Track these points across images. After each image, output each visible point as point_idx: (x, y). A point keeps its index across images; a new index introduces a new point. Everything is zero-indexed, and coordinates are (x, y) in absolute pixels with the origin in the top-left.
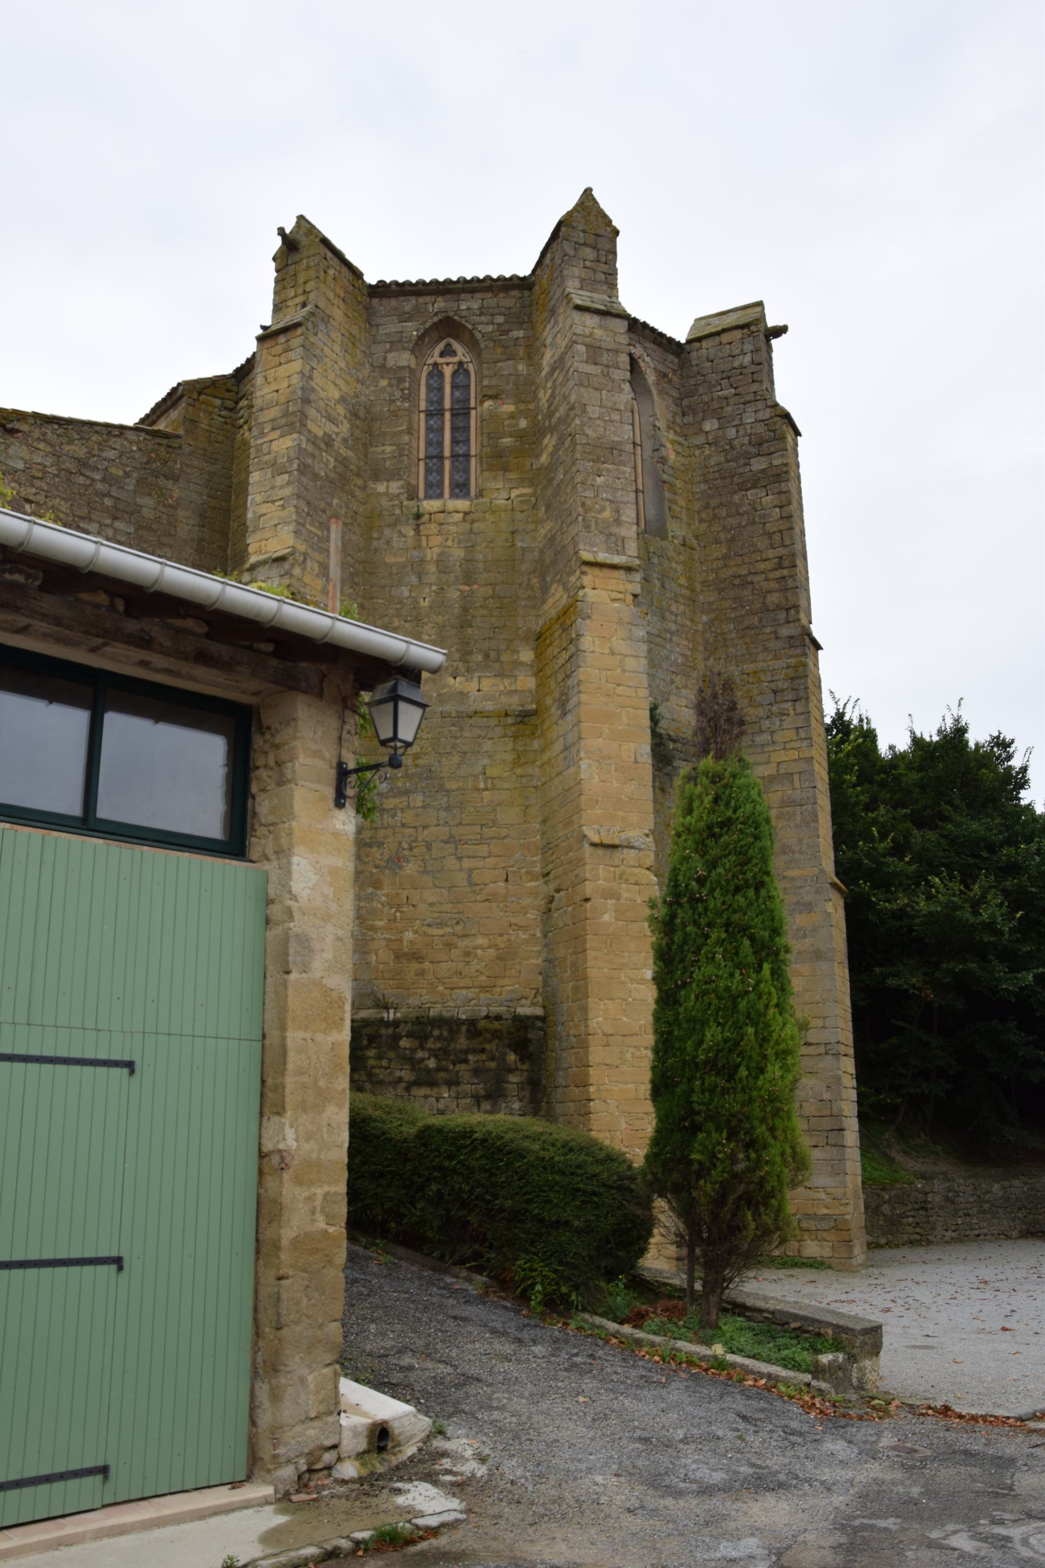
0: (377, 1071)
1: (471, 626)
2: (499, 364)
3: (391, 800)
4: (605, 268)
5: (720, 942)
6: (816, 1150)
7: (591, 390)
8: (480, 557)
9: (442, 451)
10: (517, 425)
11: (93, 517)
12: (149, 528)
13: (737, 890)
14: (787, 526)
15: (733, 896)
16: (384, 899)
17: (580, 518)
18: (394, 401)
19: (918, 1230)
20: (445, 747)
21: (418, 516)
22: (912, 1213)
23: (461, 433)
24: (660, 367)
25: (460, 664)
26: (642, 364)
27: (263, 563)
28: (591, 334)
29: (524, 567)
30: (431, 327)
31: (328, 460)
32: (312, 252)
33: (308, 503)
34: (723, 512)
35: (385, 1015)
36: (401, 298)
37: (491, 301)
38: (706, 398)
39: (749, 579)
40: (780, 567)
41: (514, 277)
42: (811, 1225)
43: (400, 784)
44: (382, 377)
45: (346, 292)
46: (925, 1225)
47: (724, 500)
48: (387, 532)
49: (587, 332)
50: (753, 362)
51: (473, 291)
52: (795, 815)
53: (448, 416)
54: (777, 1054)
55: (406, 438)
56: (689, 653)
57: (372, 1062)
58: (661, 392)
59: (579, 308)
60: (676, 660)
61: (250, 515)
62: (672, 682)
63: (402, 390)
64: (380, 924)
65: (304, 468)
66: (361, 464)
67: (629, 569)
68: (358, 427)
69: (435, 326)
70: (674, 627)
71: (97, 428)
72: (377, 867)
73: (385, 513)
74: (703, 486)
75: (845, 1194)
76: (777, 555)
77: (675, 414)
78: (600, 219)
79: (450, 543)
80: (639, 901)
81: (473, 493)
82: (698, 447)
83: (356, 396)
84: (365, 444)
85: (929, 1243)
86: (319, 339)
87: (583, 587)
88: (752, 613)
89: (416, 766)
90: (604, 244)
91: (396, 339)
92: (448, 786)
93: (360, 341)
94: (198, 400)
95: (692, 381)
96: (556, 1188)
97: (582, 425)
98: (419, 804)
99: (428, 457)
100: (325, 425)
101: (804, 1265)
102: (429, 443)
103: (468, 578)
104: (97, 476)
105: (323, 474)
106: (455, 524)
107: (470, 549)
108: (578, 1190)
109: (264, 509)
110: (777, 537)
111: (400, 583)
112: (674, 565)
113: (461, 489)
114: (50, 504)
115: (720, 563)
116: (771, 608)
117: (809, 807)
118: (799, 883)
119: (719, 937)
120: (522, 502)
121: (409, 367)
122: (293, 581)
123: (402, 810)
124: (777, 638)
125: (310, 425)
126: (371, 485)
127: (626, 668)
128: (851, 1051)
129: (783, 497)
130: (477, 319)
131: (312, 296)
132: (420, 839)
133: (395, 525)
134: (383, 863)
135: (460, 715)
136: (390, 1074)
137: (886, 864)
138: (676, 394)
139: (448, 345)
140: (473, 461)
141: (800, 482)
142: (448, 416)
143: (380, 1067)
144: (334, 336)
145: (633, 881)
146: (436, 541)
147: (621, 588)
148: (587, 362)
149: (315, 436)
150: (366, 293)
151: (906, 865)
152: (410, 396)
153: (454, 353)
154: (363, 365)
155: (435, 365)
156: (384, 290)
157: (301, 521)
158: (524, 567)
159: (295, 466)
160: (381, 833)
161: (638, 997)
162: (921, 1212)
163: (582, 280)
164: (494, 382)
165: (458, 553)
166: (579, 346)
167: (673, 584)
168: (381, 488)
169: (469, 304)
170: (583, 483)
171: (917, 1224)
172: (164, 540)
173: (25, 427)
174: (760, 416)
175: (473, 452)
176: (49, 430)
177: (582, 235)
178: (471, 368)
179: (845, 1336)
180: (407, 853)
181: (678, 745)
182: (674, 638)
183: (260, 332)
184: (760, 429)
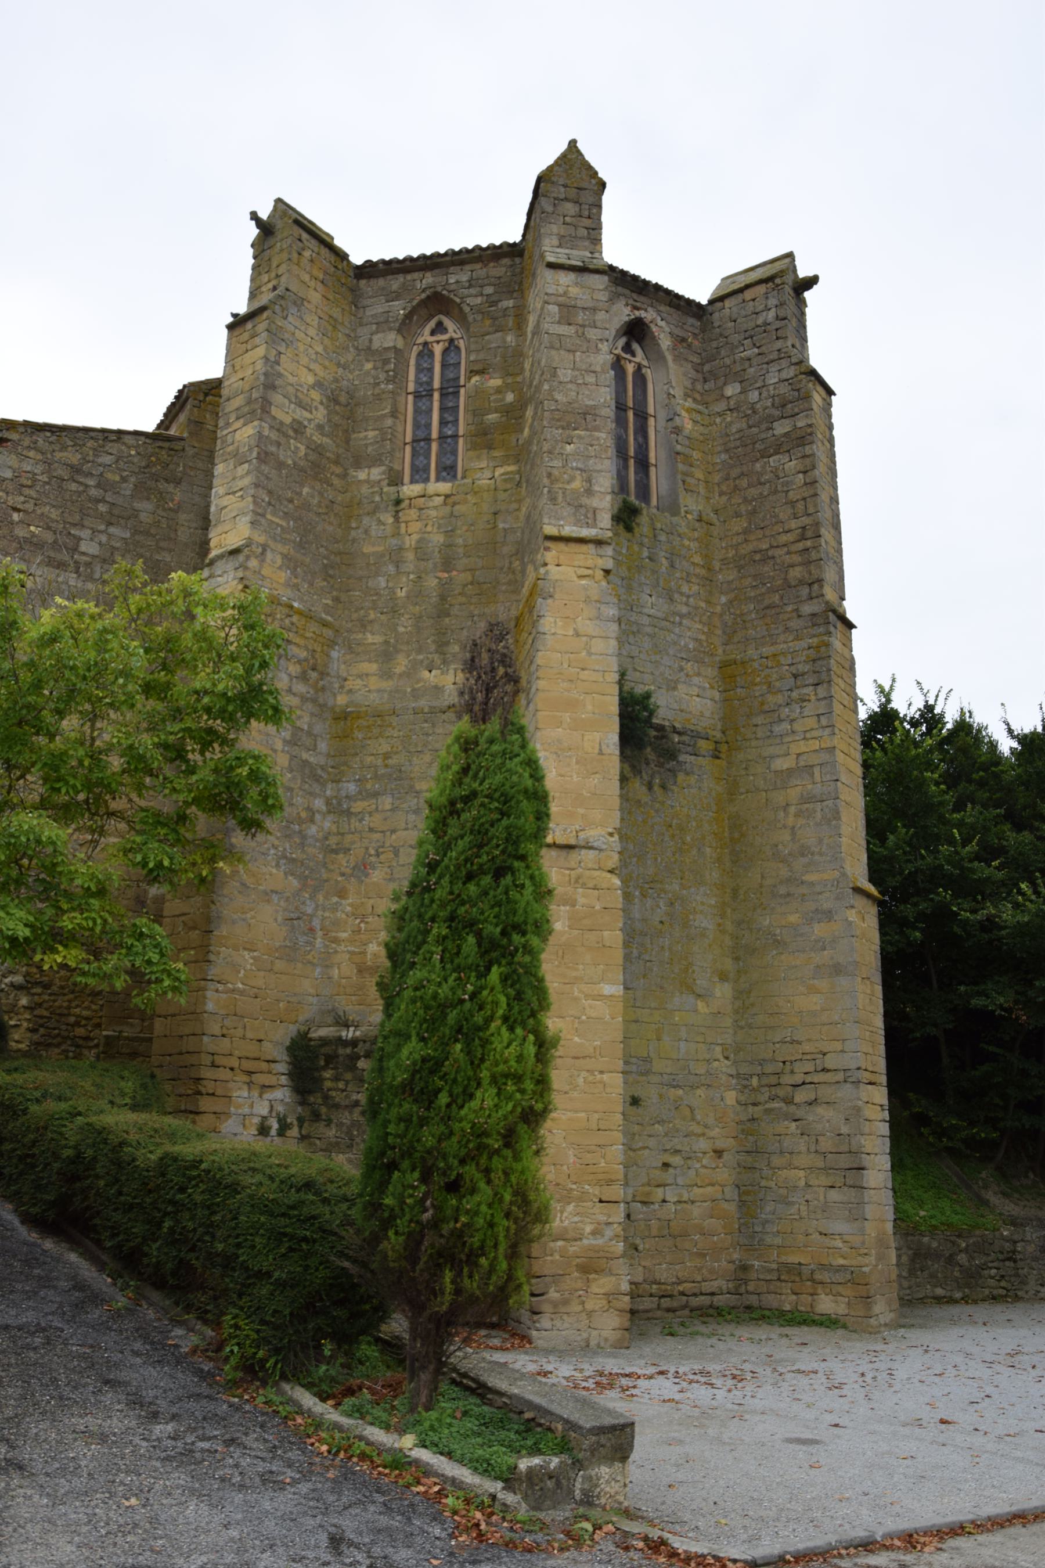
0: (333, 1093)
1: (448, 615)
2: (487, 338)
3: (359, 803)
4: (587, 222)
5: (442, 940)
6: (832, 1192)
7: (562, 352)
8: (460, 541)
9: (430, 434)
10: (503, 399)
11: (86, 523)
12: (147, 533)
13: (470, 877)
14: (812, 492)
15: (464, 883)
16: (349, 909)
17: (546, 490)
18: (378, 384)
19: (1003, 1284)
20: (416, 745)
21: (398, 502)
22: (995, 1264)
23: (449, 412)
24: (678, 331)
25: (436, 657)
26: (654, 329)
27: (220, 557)
28: (565, 293)
29: (506, 550)
30: (418, 305)
31: (297, 448)
32: (285, 234)
33: (270, 493)
34: (744, 483)
35: (344, 1034)
36: (389, 277)
37: (480, 271)
38: (728, 361)
39: (770, 553)
40: (803, 538)
41: (506, 244)
42: (825, 1277)
43: (369, 786)
44: (368, 361)
45: (326, 273)
46: (1013, 1279)
47: (745, 469)
48: (366, 520)
49: (561, 291)
50: (777, 318)
51: (462, 263)
52: (815, 812)
53: (436, 396)
54: (494, 1080)
55: (389, 422)
56: (703, 637)
57: (328, 1084)
58: (677, 358)
59: (551, 266)
60: (686, 645)
61: (213, 509)
62: (681, 669)
63: (387, 372)
64: (344, 935)
65: (264, 457)
66: (341, 451)
67: (599, 543)
68: (337, 413)
69: (423, 303)
70: (684, 610)
71: (92, 434)
72: (343, 875)
73: (365, 501)
74: (723, 456)
75: (863, 1243)
76: (800, 525)
77: (694, 381)
78: (584, 172)
79: (429, 528)
80: (597, 907)
81: (459, 475)
82: (719, 414)
83: (336, 380)
84: (347, 431)
85: (1017, 1299)
86: (291, 323)
87: (546, 564)
88: (773, 590)
89: (386, 766)
90: (587, 198)
91: (382, 319)
92: (418, 787)
93: (342, 324)
94: (204, 401)
95: (714, 344)
96: (262, 1231)
97: (551, 390)
98: (388, 807)
99: (415, 441)
100: (294, 412)
101: (814, 1323)
102: (416, 425)
103: (447, 564)
104: (91, 482)
105: (290, 462)
106: (435, 508)
107: (450, 533)
108: (285, 1235)
109: (226, 501)
110: (800, 506)
111: (377, 574)
112: (686, 542)
113: (448, 471)
114: (39, 512)
115: (741, 538)
116: (793, 584)
117: (830, 803)
118: (818, 889)
119: (439, 934)
120: (505, 480)
121: (395, 347)
122: (248, 573)
123: (370, 814)
124: (799, 616)
125: (274, 411)
126: (352, 472)
127: (593, 650)
128: (884, 1079)
129: (807, 461)
130: (466, 292)
131: (283, 279)
132: (387, 844)
133: (374, 512)
134: (348, 871)
135: (433, 711)
136: (346, 1097)
137: (972, 871)
138: (696, 359)
139: (440, 324)
140: (461, 441)
141: (833, 445)
142: (436, 396)
143: (337, 1089)
144: (308, 320)
145: (591, 885)
146: (415, 527)
147: (590, 563)
148: (559, 323)
149: (282, 423)
150: (352, 274)
151: (992, 871)
152: (397, 377)
153: (445, 330)
154: (347, 348)
155: (426, 344)
156: (371, 270)
157: (260, 511)
158: (506, 550)
159: (255, 454)
160: (349, 838)
161: (593, 1015)
162: (1007, 1263)
163: (561, 237)
164: (481, 356)
165: (438, 539)
166: (550, 307)
167: (684, 563)
168: (362, 475)
169: (458, 277)
170: (550, 452)
171: (1003, 1276)
172: (162, 544)
173: (14, 436)
174: (784, 375)
175: (461, 433)
176: (40, 439)
177: (562, 189)
178: (462, 344)
179: (574, 1435)
180: (373, 859)
181: (685, 738)
182: (684, 622)
183: (231, 319)
184: (784, 389)
